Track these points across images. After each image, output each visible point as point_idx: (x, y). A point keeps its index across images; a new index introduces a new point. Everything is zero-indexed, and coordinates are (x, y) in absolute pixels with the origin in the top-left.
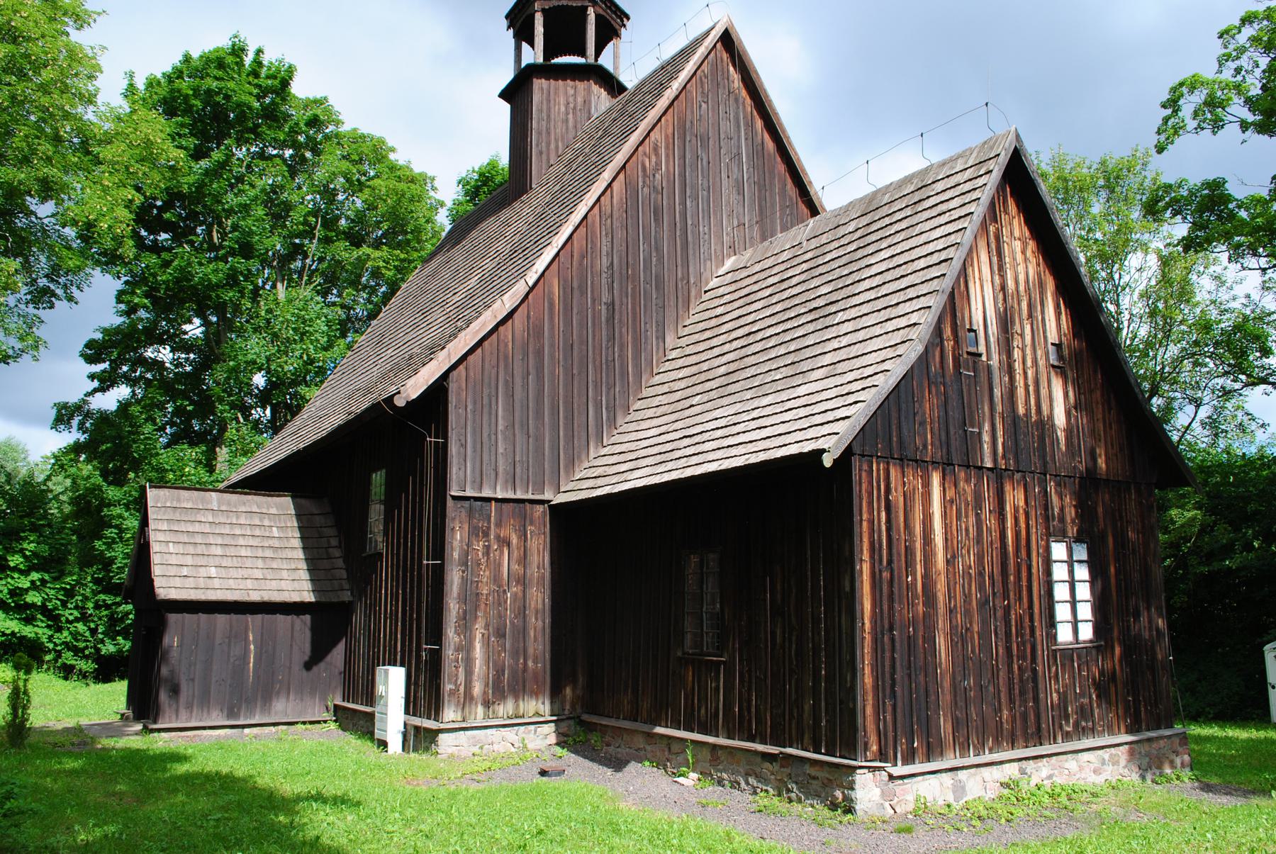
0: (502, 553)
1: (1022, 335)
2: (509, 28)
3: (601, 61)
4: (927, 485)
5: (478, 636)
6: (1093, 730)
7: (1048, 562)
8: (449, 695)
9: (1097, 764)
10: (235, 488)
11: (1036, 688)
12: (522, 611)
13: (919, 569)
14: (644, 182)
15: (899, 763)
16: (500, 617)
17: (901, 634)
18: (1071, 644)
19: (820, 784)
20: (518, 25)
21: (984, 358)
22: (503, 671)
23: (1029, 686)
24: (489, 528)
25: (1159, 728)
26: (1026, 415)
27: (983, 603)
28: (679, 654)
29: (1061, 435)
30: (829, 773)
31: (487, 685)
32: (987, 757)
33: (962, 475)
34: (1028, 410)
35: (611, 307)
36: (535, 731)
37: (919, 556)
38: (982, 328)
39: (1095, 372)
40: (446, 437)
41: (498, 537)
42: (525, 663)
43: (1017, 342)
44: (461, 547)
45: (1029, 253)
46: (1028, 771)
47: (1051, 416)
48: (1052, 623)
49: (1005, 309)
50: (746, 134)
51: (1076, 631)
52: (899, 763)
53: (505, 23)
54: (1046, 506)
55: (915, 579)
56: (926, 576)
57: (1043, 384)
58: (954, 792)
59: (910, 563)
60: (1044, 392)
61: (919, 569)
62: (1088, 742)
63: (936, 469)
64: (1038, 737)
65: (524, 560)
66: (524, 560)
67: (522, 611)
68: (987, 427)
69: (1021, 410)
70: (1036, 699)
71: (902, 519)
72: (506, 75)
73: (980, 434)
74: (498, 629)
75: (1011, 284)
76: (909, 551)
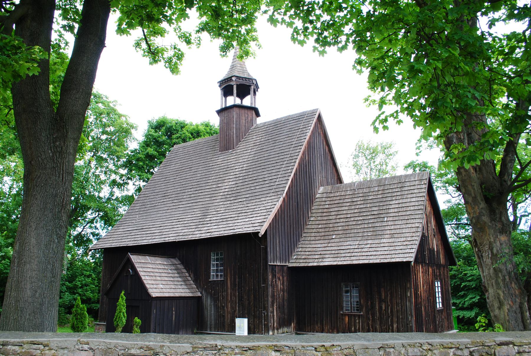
28: (342, 313)
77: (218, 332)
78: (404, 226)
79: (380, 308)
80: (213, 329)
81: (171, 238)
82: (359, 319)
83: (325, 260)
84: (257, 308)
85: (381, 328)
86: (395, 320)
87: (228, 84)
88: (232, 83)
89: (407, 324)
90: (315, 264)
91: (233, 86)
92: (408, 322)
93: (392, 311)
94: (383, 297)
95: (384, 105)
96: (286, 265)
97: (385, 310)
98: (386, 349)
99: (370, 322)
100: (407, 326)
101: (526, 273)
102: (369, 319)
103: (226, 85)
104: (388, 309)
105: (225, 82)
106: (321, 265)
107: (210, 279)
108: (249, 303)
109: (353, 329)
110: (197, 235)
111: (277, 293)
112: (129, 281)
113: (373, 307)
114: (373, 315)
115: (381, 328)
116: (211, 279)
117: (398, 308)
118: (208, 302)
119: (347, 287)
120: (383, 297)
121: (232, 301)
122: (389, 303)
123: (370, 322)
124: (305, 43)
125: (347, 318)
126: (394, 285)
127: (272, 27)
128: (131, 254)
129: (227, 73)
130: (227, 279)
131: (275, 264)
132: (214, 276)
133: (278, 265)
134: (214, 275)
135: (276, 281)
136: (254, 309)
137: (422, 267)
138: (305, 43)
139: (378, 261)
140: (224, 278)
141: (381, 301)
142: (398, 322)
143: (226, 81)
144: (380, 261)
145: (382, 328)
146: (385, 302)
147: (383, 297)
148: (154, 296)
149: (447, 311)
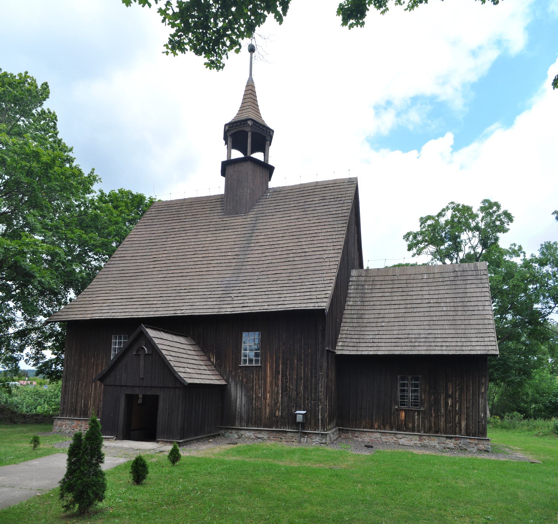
28: (396, 407)
77: (252, 427)
78: (392, 320)
79: (447, 403)
80: (243, 424)
81: (187, 311)
82: (418, 415)
83: (381, 348)
84: (308, 399)
85: (446, 425)
86: (464, 417)
87: (241, 129)
88: (247, 129)
89: (479, 422)
91: (247, 132)
92: (480, 420)
94: (450, 392)
97: (452, 406)
98: (243, 432)
99: (433, 420)
100: (478, 424)
102: (431, 415)
103: (237, 130)
105: (236, 126)
107: (240, 364)
109: (410, 425)
110: (227, 310)
111: (260, 382)
112: (142, 362)
113: (437, 402)
114: (437, 411)
115: (446, 425)
116: (242, 365)
117: (468, 405)
119: (403, 379)
120: (450, 393)
121: (272, 392)
123: (433, 420)
126: (465, 379)
128: (146, 327)
129: (233, 118)
130: (266, 365)
134: (246, 360)
136: (304, 401)
139: (454, 353)
140: (261, 363)
141: (447, 396)
142: (467, 419)
143: (235, 125)
145: (448, 425)
146: (452, 398)
147: (450, 393)
148: (189, 381)
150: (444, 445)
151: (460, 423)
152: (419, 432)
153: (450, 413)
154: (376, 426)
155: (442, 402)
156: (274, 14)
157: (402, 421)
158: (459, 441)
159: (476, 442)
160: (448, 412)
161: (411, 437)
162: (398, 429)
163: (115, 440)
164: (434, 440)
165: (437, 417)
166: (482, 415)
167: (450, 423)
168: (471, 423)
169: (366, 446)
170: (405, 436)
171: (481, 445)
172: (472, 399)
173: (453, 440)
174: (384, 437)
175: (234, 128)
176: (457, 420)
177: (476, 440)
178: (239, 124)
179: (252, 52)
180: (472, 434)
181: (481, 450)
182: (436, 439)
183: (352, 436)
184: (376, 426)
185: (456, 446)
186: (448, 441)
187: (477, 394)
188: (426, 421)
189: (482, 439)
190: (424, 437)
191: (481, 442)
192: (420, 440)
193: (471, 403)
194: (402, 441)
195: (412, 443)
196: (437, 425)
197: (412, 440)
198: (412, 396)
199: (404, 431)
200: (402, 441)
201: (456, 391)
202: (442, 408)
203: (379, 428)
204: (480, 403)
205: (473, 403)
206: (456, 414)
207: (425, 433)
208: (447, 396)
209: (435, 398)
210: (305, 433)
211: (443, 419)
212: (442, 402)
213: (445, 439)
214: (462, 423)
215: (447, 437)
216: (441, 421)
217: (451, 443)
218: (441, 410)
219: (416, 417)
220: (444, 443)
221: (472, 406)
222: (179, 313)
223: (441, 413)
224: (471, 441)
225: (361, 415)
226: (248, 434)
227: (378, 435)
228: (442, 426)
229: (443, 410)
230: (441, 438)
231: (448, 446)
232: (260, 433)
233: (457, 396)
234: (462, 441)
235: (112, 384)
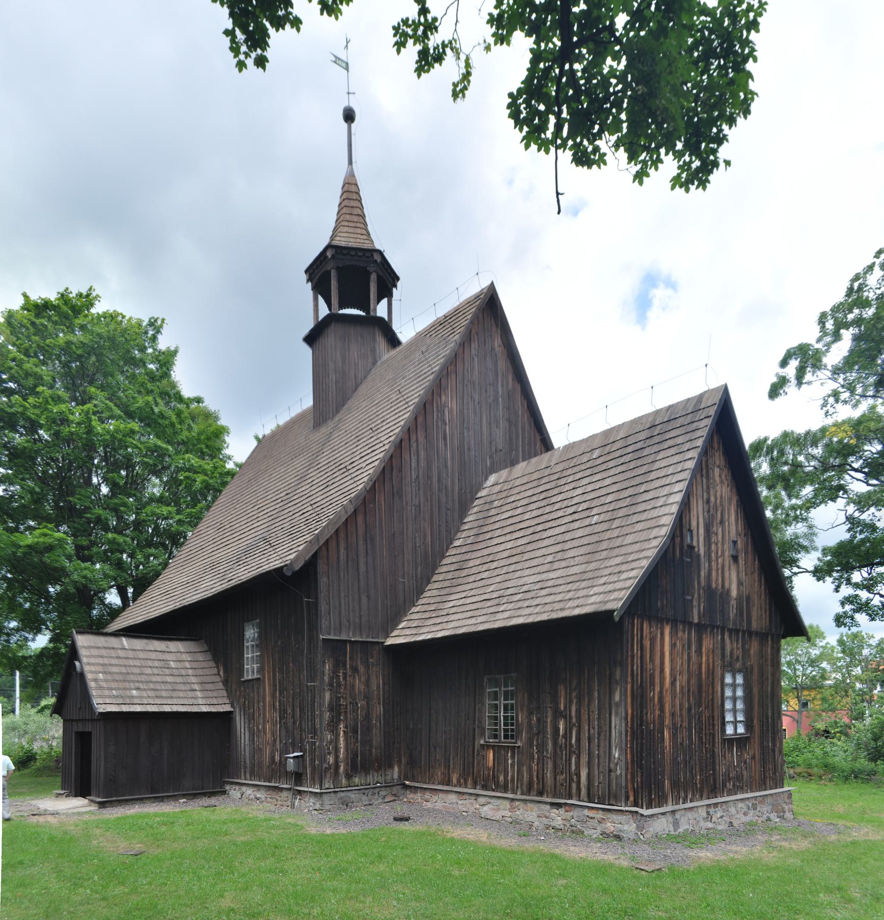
0: (354, 678)
1: (716, 534)
2: (308, 281)
3: (333, 311)
4: (662, 634)
5: (342, 734)
6: (742, 788)
7: (723, 685)
8: (325, 772)
9: (745, 809)
10: (135, 631)
11: (714, 762)
12: (367, 717)
13: (657, 689)
14: (438, 416)
15: (645, 807)
16: (355, 720)
17: (646, 728)
18: (733, 735)
19: (596, 821)
20: (316, 279)
21: (696, 549)
22: (357, 755)
23: (710, 762)
24: (346, 661)
25: (776, 788)
26: (716, 588)
27: (689, 709)
28: (482, 742)
29: (733, 603)
30: (603, 815)
31: (348, 764)
32: (689, 805)
33: (681, 627)
34: (717, 585)
35: (418, 508)
36: (378, 793)
37: (657, 680)
38: (696, 529)
39: (754, 560)
40: (317, 598)
41: (352, 667)
42: (370, 751)
43: (713, 539)
44: (329, 674)
45: (723, 477)
46: (711, 813)
47: (729, 591)
48: (724, 724)
49: (709, 517)
50: (502, 382)
51: (736, 729)
52: (645, 807)
53: (304, 277)
54: (723, 648)
55: (654, 694)
56: (661, 692)
57: (726, 568)
58: (673, 826)
59: (653, 684)
60: (727, 574)
61: (657, 689)
62: (740, 796)
63: (667, 624)
64: (714, 791)
65: (368, 683)
66: (368, 683)
67: (367, 717)
68: (696, 596)
69: (714, 586)
70: (714, 769)
71: (648, 656)
72: (309, 325)
73: (692, 600)
74: (353, 728)
75: (712, 499)
76: (652, 676)
79: (556, 730)
85: (555, 779)
89: (610, 771)
90: (429, 636)
93: (578, 740)
95: (605, 158)
96: (378, 643)
97: (565, 736)
99: (535, 767)
100: (609, 775)
101: (117, 373)
104: (571, 733)
106: (437, 636)
107: (243, 677)
108: (294, 723)
114: (542, 746)
115: (555, 779)
117: (592, 731)
118: (240, 724)
122: (574, 720)
123: (535, 767)
124: (402, 20)
125: (491, 755)
127: (506, 106)
131: (344, 637)
132: (251, 669)
133: (350, 642)
135: (345, 674)
137: (674, 633)
138: (402, 20)
139: (544, 617)
143: (314, 267)
144: (548, 616)
145: (558, 777)
146: (565, 717)
149: (762, 743)
150: (546, 821)
151: (578, 776)
152: (514, 792)
153: (562, 752)
154: (455, 781)
155: (549, 729)
156: (628, 18)
157: (489, 769)
158: (571, 814)
159: (600, 815)
160: (558, 750)
161: (499, 802)
162: (485, 787)
163: (67, 796)
164: (532, 810)
165: (542, 761)
166: (617, 755)
167: (562, 773)
168: (596, 772)
169: (396, 819)
170: (489, 800)
171: (609, 824)
172: (599, 718)
173: (562, 811)
174: (460, 802)
175: (317, 271)
176: (573, 767)
177: (601, 812)
178: (318, 263)
179: (350, 122)
180: (599, 798)
181: (608, 836)
182: (535, 807)
183: (422, 799)
184: (455, 781)
185: (565, 823)
186: (554, 812)
187: (607, 706)
188: (525, 768)
189: (609, 810)
190: (517, 803)
191: (609, 815)
192: (512, 810)
193: (596, 727)
194: (486, 811)
195: (498, 816)
196: (542, 779)
197: (499, 809)
198: (506, 718)
199: (493, 790)
200: (486, 811)
201: (571, 702)
202: (550, 741)
203: (459, 784)
204: (613, 726)
205: (599, 727)
206: (571, 753)
207: (522, 794)
208: (558, 714)
209: (538, 720)
210: (300, 792)
211: (550, 765)
212: (549, 729)
213: (548, 807)
214: (582, 774)
215: (552, 804)
216: (547, 768)
217: (558, 817)
218: (547, 744)
219: (510, 761)
220: (547, 817)
221: (599, 734)
222: (186, 602)
223: (547, 752)
224: (591, 814)
225: (435, 760)
226: (249, 791)
227: (453, 798)
228: (549, 780)
229: (550, 746)
230: (543, 806)
231: (553, 824)
232: (259, 790)
233: (573, 714)
234: (576, 813)
235: (87, 718)
